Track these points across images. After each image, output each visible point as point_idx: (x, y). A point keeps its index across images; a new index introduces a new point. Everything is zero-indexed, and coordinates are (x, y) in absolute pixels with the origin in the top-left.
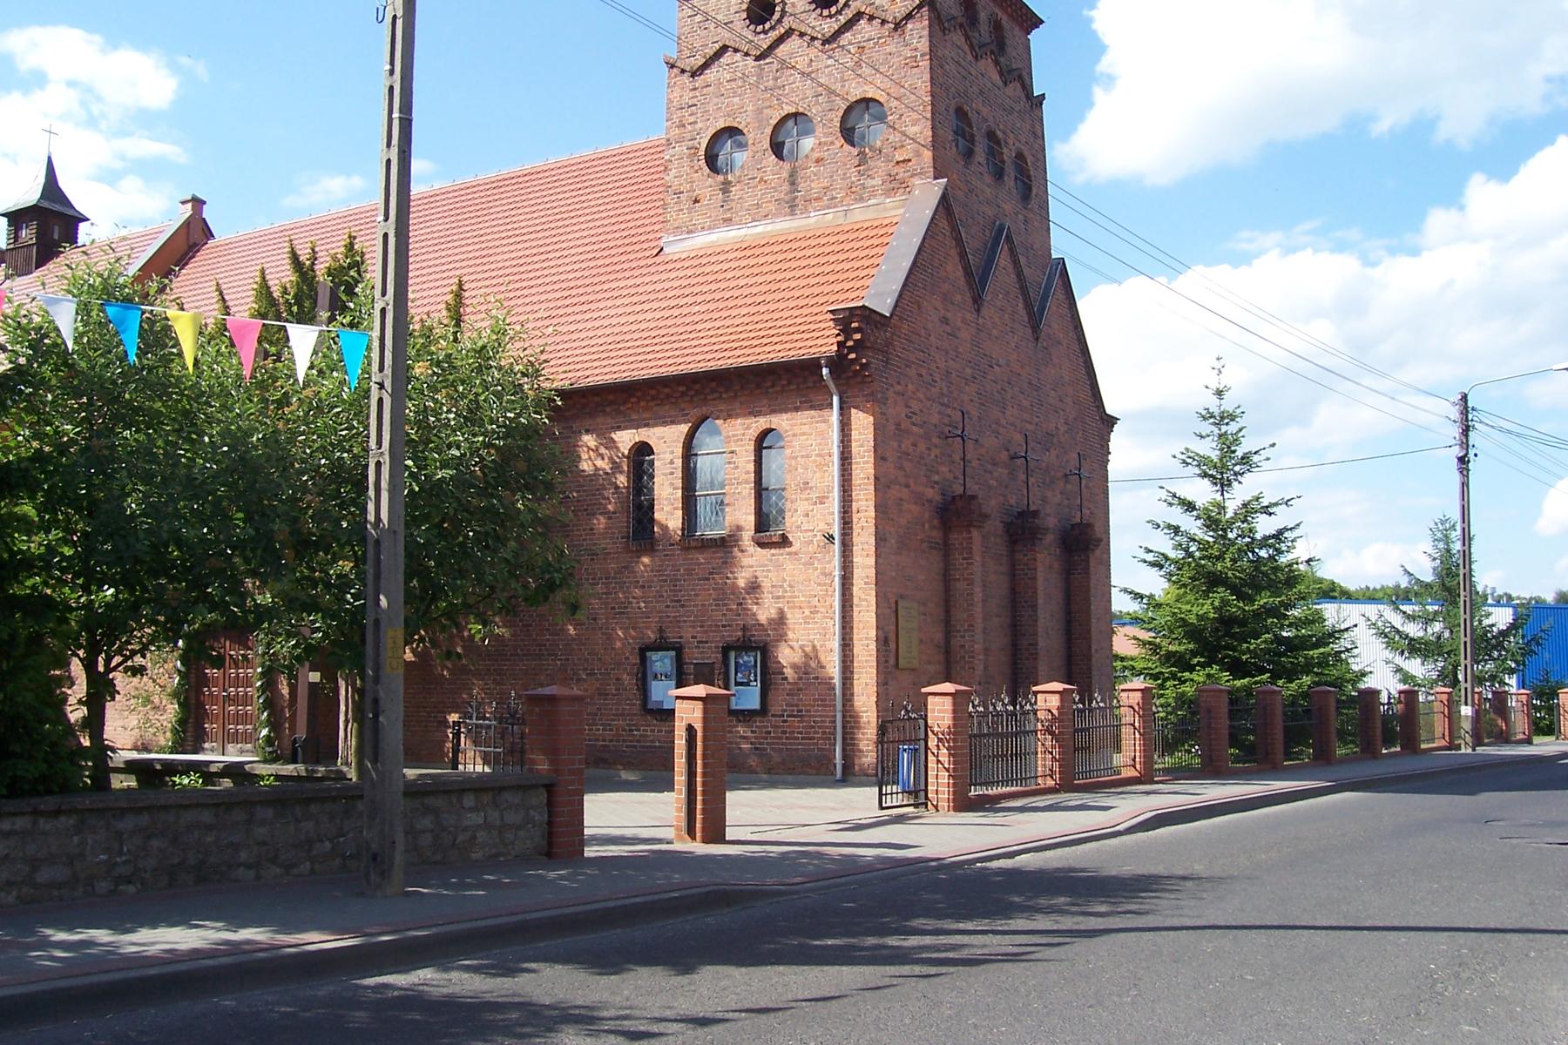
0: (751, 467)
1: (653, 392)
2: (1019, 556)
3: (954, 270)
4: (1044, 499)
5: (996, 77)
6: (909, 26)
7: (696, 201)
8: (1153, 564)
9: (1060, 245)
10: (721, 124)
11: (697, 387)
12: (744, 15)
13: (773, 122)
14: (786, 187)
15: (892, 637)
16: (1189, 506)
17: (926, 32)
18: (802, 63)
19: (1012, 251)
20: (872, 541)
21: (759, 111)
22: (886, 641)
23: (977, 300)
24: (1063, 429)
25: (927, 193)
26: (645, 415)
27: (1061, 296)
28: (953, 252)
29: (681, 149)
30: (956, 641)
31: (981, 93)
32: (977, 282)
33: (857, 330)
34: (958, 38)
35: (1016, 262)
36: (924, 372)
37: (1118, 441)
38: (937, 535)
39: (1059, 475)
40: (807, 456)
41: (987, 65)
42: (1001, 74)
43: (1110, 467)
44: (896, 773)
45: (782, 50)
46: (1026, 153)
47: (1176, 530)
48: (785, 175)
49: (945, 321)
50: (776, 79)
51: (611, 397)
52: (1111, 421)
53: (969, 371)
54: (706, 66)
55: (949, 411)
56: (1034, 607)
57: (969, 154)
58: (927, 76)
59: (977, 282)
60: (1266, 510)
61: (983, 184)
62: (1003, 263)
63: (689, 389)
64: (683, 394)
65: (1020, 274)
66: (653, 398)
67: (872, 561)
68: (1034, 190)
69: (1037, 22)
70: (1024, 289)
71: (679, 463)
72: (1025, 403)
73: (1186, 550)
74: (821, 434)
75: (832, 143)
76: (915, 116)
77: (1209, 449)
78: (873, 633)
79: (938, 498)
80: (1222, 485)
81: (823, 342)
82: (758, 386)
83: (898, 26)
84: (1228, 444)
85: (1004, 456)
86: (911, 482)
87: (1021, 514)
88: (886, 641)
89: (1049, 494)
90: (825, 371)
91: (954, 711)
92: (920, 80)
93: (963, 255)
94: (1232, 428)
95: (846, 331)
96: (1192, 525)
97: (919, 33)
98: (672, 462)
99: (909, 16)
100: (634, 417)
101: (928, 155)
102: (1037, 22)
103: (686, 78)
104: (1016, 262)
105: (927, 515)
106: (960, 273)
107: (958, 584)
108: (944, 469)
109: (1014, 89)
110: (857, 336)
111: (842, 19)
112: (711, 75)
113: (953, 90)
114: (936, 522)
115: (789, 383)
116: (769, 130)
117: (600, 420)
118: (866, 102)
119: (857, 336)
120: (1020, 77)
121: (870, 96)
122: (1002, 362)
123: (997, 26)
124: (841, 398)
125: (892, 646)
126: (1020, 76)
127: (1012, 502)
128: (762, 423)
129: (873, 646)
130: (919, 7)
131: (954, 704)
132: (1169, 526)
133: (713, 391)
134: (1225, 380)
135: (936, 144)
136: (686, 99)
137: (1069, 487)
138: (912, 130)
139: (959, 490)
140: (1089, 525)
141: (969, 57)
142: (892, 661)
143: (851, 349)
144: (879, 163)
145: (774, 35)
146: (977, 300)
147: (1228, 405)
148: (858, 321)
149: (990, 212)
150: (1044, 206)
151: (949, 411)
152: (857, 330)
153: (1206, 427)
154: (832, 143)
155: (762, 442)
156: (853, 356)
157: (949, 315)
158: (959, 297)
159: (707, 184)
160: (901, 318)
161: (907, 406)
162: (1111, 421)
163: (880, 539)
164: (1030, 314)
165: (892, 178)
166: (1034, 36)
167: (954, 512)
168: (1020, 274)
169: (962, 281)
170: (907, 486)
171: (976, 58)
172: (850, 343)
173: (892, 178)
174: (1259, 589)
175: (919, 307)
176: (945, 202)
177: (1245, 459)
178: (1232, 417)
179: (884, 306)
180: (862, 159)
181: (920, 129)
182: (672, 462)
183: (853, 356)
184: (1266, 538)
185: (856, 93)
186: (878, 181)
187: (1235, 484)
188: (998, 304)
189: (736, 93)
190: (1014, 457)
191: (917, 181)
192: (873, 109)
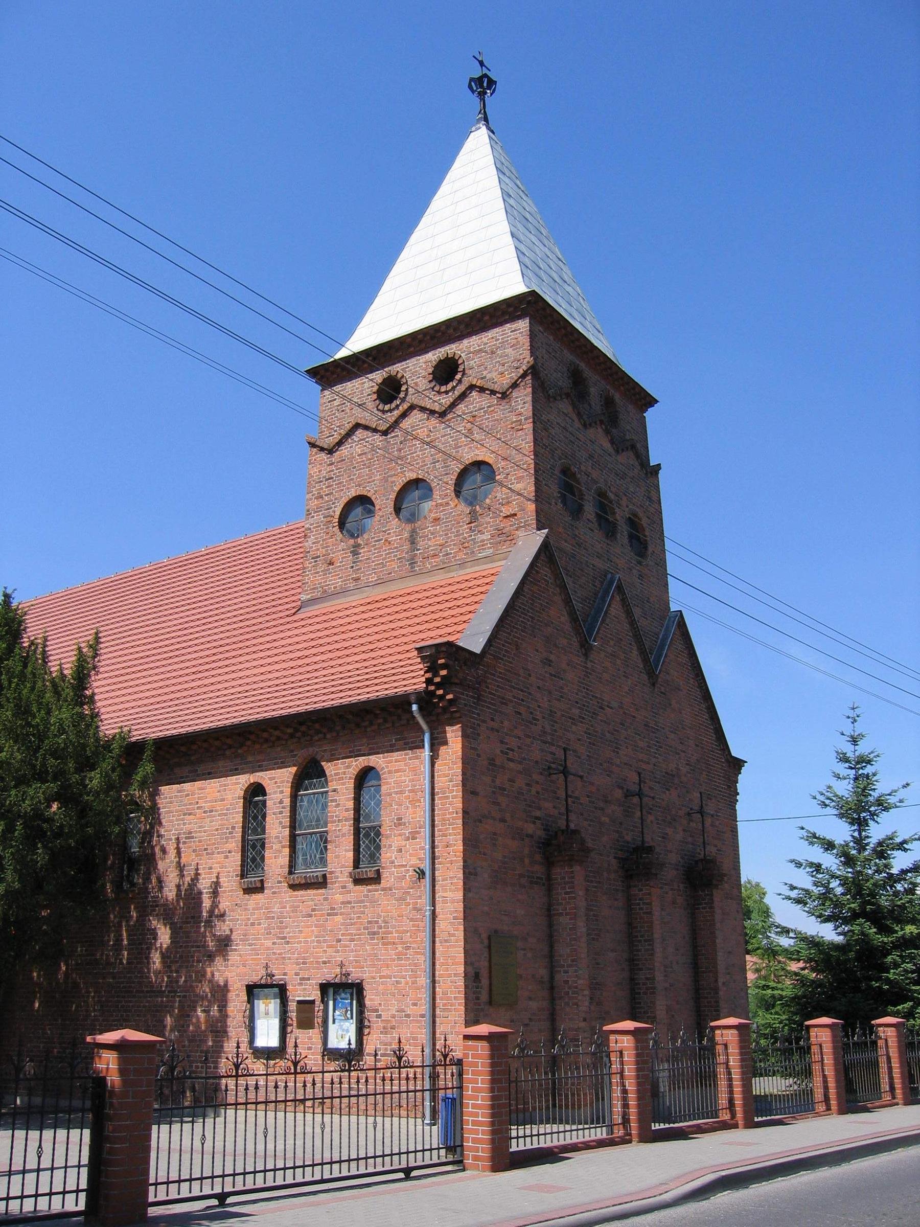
0: (351, 805)
1: (265, 735)
2: (634, 891)
3: (558, 616)
4: (665, 837)
5: (607, 445)
6: (514, 394)
7: (331, 563)
8: (798, 901)
9: (679, 598)
10: (353, 493)
11: (303, 728)
12: (375, 396)
13: (397, 489)
14: (406, 547)
15: (484, 974)
16: (829, 846)
17: (529, 399)
18: (422, 433)
19: (624, 601)
20: (461, 875)
21: (385, 479)
22: (477, 976)
23: (586, 648)
24: (684, 769)
25: (530, 541)
26: (259, 757)
27: (680, 645)
28: (558, 599)
29: (319, 517)
30: (560, 977)
31: (591, 457)
32: (584, 628)
33: (444, 666)
34: (565, 406)
35: (629, 613)
36: (522, 710)
37: (744, 781)
38: (539, 870)
39: (681, 813)
40: (401, 792)
41: (599, 439)
42: (612, 442)
43: (738, 807)
44: (600, 1090)
45: (406, 424)
46: (641, 514)
47: (818, 867)
48: (406, 535)
49: (548, 662)
50: (400, 450)
51: (229, 741)
52: (737, 765)
53: (576, 711)
54: (340, 443)
55: (553, 749)
56: (650, 941)
57: (577, 512)
58: (530, 438)
59: (584, 628)
60: (901, 846)
61: (593, 537)
62: (613, 612)
63: (296, 730)
64: (292, 736)
65: (633, 623)
66: (266, 741)
67: (460, 896)
68: (650, 549)
69: (648, 401)
70: (637, 637)
71: (287, 802)
72: (641, 744)
73: (826, 886)
74: (414, 770)
75: (447, 504)
76: (521, 473)
77: (844, 789)
78: (461, 969)
79: (540, 833)
80: (860, 825)
81: (412, 679)
82: (358, 725)
83: (504, 395)
84: (863, 784)
85: (619, 794)
86: (508, 816)
87: (636, 850)
88: (477, 976)
89: (669, 831)
90: (415, 707)
91: (492, 1057)
92: (525, 441)
93: (568, 601)
94: (869, 770)
95: (433, 669)
96: (830, 861)
97: (523, 400)
98: (281, 802)
99: (515, 385)
100: (250, 759)
101: (531, 507)
102: (648, 401)
103: (323, 455)
104: (629, 613)
105: (526, 851)
106: (565, 618)
107: (561, 919)
108: (547, 805)
109: (626, 458)
110: (444, 672)
111: (457, 393)
112: (344, 451)
113: (558, 452)
114: (538, 857)
115: (385, 721)
116: (393, 496)
117: (221, 763)
118: (479, 465)
119: (444, 672)
120: (633, 447)
121: (480, 458)
122: (615, 704)
123: (609, 402)
124: (432, 735)
125: (485, 982)
126: (636, 447)
127: (629, 838)
128: (362, 762)
129: (461, 983)
130: (523, 376)
131: (492, 1049)
132: (811, 864)
133: (318, 732)
134: (859, 729)
135: (540, 497)
136: (324, 473)
137: (693, 825)
138: (518, 487)
139: (562, 824)
140: (713, 861)
141: (577, 424)
142: (484, 997)
143: (438, 686)
144: (488, 519)
145: (396, 413)
146: (586, 648)
147: (863, 748)
148: (444, 658)
149: (600, 564)
150: (662, 563)
151: (553, 749)
152: (444, 666)
153: (842, 769)
154: (447, 504)
155: (364, 777)
156: (440, 692)
157: (552, 657)
158: (565, 641)
159: (339, 546)
160: (496, 658)
161: (502, 742)
162: (737, 765)
163: (469, 873)
164: (646, 661)
165: (500, 532)
166: (650, 415)
167: (556, 847)
168: (633, 623)
169: (568, 627)
170: (503, 820)
171: (585, 425)
172: (437, 680)
173: (500, 532)
174: (902, 921)
175: (517, 647)
176: (545, 547)
177: (879, 802)
178: (869, 762)
179: (476, 645)
180: (474, 517)
181: (527, 485)
182: (281, 802)
183: (440, 692)
184: (904, 872)
185: (469, 455)
186: (486, 536)
187: (871, 822)
188: (610, 650)
189: (371, 468)
190: (628, 794)
191: (521, 533)
192: (485, 470)
